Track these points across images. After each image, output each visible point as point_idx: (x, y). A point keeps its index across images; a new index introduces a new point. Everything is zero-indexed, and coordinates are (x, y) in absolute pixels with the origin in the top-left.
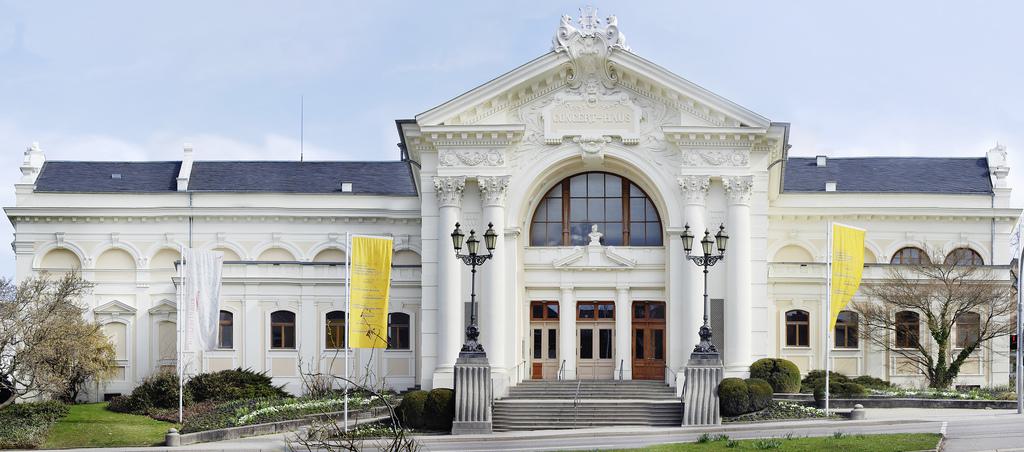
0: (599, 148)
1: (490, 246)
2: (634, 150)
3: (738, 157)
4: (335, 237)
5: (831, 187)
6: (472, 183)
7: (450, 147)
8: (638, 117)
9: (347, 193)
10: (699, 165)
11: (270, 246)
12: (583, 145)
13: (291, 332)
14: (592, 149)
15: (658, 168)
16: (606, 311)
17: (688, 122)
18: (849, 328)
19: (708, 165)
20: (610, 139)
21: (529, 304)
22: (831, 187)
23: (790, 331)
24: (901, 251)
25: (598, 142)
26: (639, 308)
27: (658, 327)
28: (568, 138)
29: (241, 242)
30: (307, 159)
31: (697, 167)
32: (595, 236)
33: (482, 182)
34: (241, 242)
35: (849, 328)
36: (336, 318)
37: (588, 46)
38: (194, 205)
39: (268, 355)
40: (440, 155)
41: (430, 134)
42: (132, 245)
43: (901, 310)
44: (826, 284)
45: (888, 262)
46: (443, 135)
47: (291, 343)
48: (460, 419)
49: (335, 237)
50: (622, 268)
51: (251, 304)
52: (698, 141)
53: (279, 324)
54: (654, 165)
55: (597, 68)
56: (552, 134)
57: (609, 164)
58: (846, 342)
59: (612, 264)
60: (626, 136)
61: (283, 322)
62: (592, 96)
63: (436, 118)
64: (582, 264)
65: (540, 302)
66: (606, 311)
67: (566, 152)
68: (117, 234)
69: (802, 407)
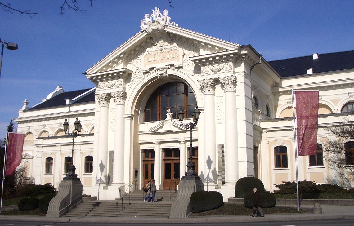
2: (180, 70)
3: (227, 66)
5: (310, 72)
6: (217, 81)
8: (181, 54)
9: (310, 75)
11: (287, 106)
13: (285, 158)
14: (161, 72)
16: (176, 151)
17: (204, 53)
19: (213, 73)
20: (170, 66)
24: (346, 105)
25: (164, 68)
27: (176, 162)
28: (152, 69)
29: (330, 100)
31: (208, 72)
32: (169, 115)
34: (330, 100)
35: (318, 154)
36: (89, 159)
37: (155, 26)
38: (71, 110)
39: (273, 172)
40: (99, 85)
42: (328, 101)
43: (348, 140)
44: (294, 130)
45: (339, 111)
47: (285, 165)
48: (50, 209)
51: (58, 155)
53: (88, 162)
55: (162, 34)
57: (171, 78)
58: (316, 162)
59: (177, 129)
60: (176, 64)
62: (161, 48)
65: (169, 149)
66: (176, 151)
67: (153, 75)
69: (177, 205)
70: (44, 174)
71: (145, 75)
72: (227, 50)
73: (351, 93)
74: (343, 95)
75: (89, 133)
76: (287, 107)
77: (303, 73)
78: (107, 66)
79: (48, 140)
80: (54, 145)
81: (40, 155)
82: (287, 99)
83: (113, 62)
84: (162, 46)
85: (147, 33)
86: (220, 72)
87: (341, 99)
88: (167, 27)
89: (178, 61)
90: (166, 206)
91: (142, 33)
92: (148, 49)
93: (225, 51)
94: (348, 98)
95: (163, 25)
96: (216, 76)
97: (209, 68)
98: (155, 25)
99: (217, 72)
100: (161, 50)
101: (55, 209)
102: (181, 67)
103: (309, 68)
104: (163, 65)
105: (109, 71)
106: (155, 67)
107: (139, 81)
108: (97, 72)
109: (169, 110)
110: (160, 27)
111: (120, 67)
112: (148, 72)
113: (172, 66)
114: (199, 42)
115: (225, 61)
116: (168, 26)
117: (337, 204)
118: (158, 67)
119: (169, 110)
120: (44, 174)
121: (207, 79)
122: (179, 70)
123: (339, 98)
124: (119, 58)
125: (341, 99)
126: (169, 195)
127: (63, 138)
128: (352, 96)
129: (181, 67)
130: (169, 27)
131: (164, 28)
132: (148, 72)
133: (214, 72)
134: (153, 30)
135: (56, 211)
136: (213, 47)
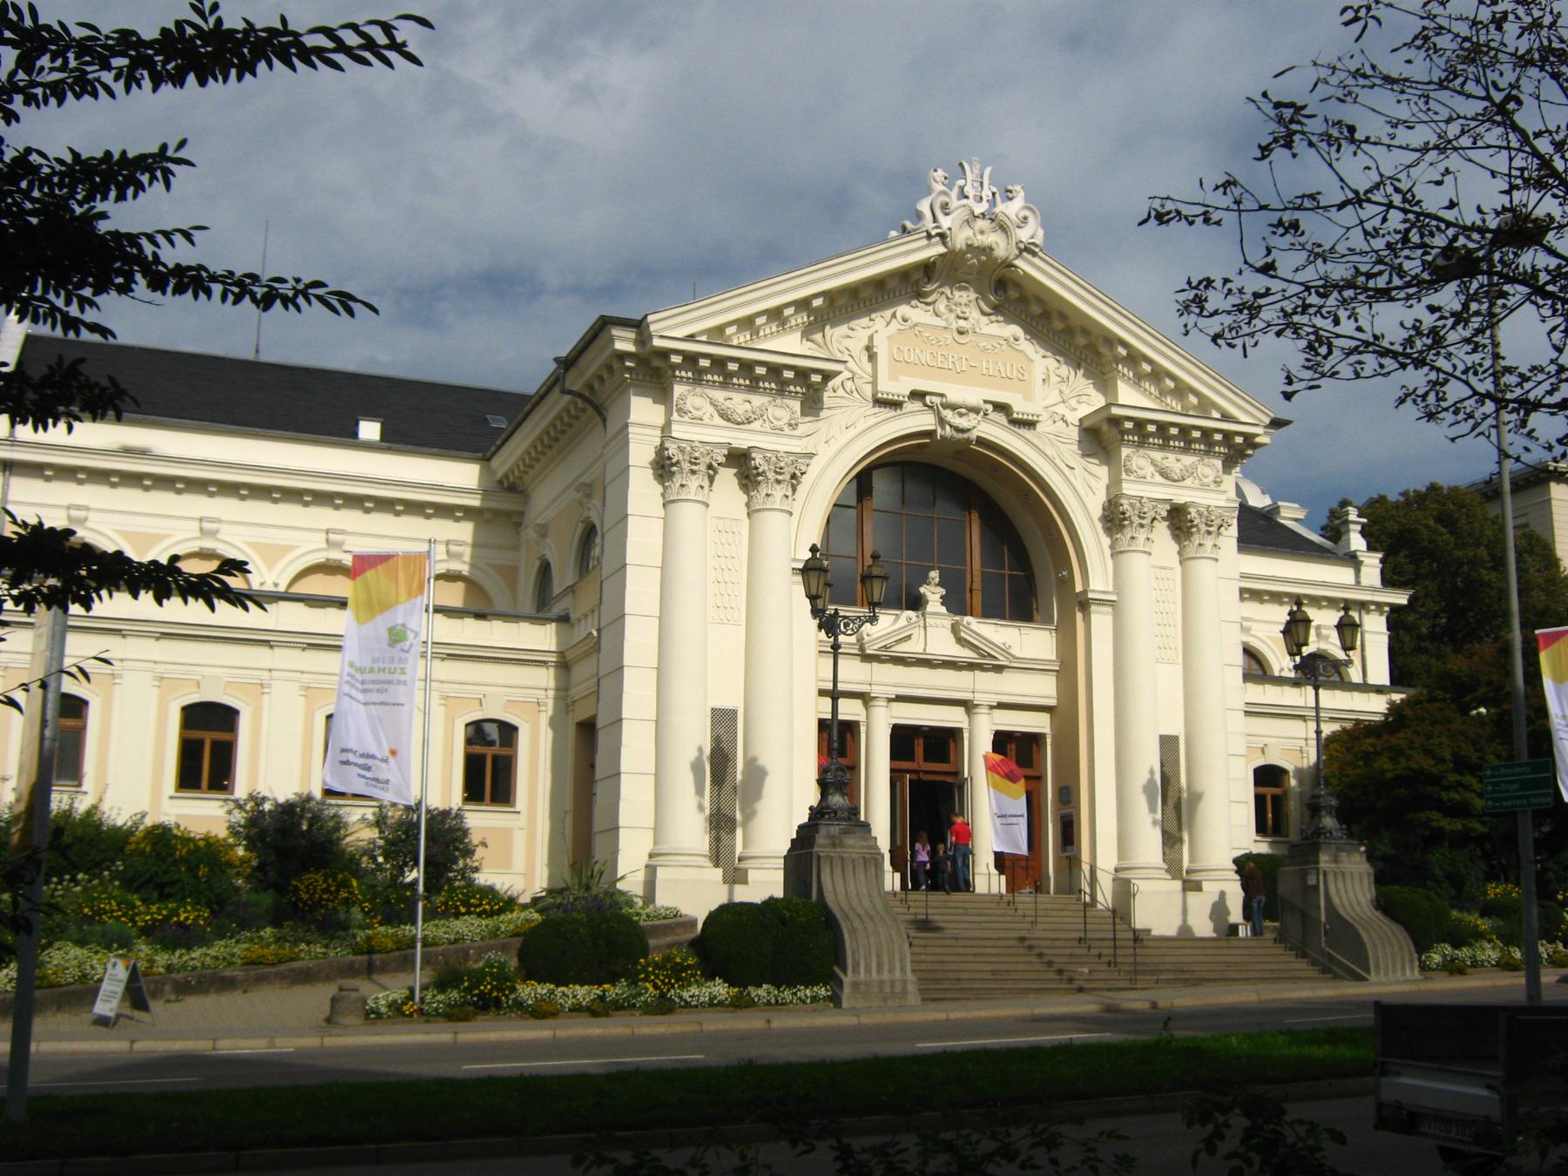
0: (974, 423)
1: (1349, 645)
2: (1024, 432)
3: (779, 413)
4: (82, 514)
5: (370, 430)
6: (740, 460)
7: (698, 380)
8: (1038, 375)
9: (368, 446)
10: (1149, 479)
11: (319, 558)
12: (948, 415)
14: (962, 422)
15: (1067, 471)
16: (943, 742)
17: (1132, 398)
18: (495, 758)
21: (709, 713)
22: (370, 430)
23: (189, 755)
26: (903, 738)
28: (918, 395)
29: (120, 532)
30: (270, 356)
33: (758, 459)
37: (982, 232)
41: (665, 354)
42: (238, 543)
46: (691, 359)
48: (856, 970)
49: (82, 514)
50: (988, 663)
52: (1143, 432)
53: (195, 734)
54: (1063, 466)
56: (891, 387)
60: (1020, 408)
61: (206, 728)
62: (962, 323)
63: (683, 324)
64: (913, 648)
67: (917, 420)
68: (342, 532)
70: (171, 798)
71: (886, 413)
72: (1226, 417)
73: (79, 507)
74: (308, 535)
75: (282, 588)
76: (197, 549)
77: (345, 434)
78: (747, 323)
79: (1364, 696)
80: (263, 640)
81: (1239, 746)
82: (69, 507)
83: (775, 314)
84: (965, 319)
85: (942, 250)
86: (752, 426)
87: (290, 548)
88: (1029, 257)
89: (1028, 397)
90: (942, 996)
91: (925, 242)
92: (903, 310)
93: (1218, 416)
94: (315, 547)
95: (1022, 246)
96: (741, 440)
97: (1153, 463)
98: (984, 228)
99: (743, 423)
100: (961, 333)
101: (879, 970)
102: (1030, 424)
103: (371, 415)
104: (973, 397)
105: (738, 347)
106: (942, 395)
107: (852, 432)
108: (691, 338)
109: (934, 575)
110: (1002, 248)
111: (788, 345)
112: (895, 405)
113: (1001, 408)
114: (1134, 358)
115: (782, 389)
116: (1034, 254)
117: (1274, 1000)
118: (954, 396)
119: (934, 575)
120: (171, 798)
121: (1151, 500)
122: (1020, 431)
123: (158, 531)
124: (803, 305)
125: (290, 548)
126: (1138, 951)
127: (311, 606)
128: (213, 534)
129: (1030, 424)
130: (1036, 260)
131: (1017, 257)
132: (895, 405)
133: (729, 420)
134: (969, 246)
135: (898, 975)
136: (1181, 390)
